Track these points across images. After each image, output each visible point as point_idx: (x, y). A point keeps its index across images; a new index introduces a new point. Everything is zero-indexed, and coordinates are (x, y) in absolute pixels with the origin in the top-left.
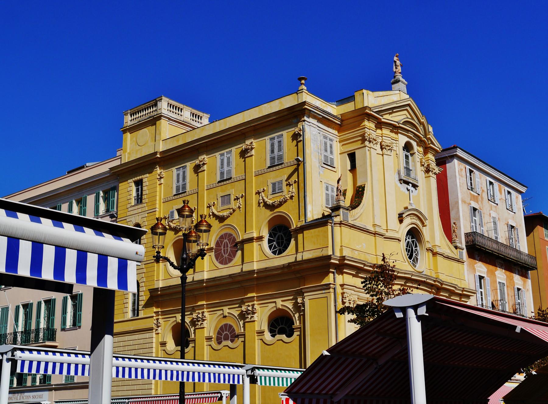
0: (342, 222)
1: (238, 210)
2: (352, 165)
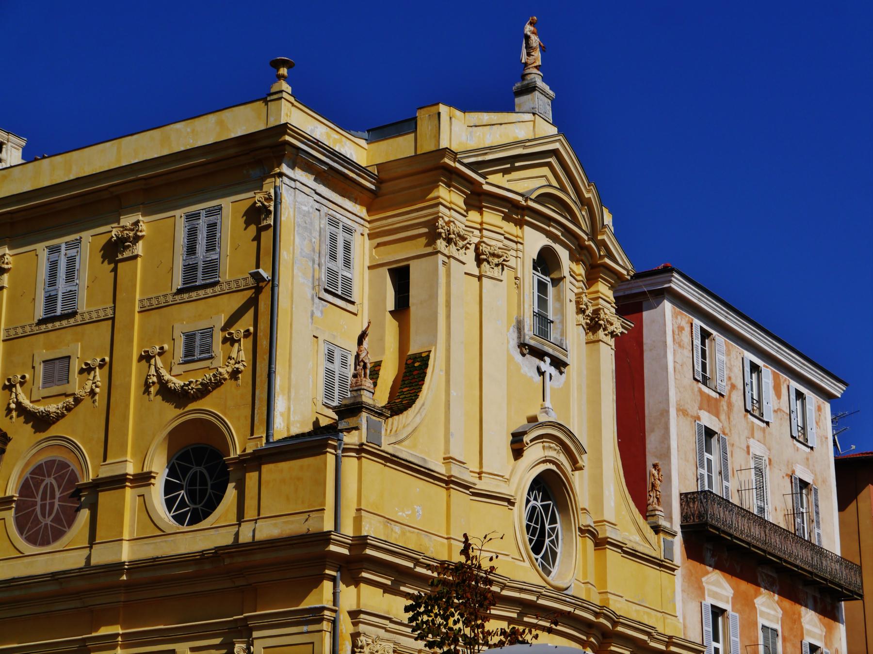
1: (88, 400)
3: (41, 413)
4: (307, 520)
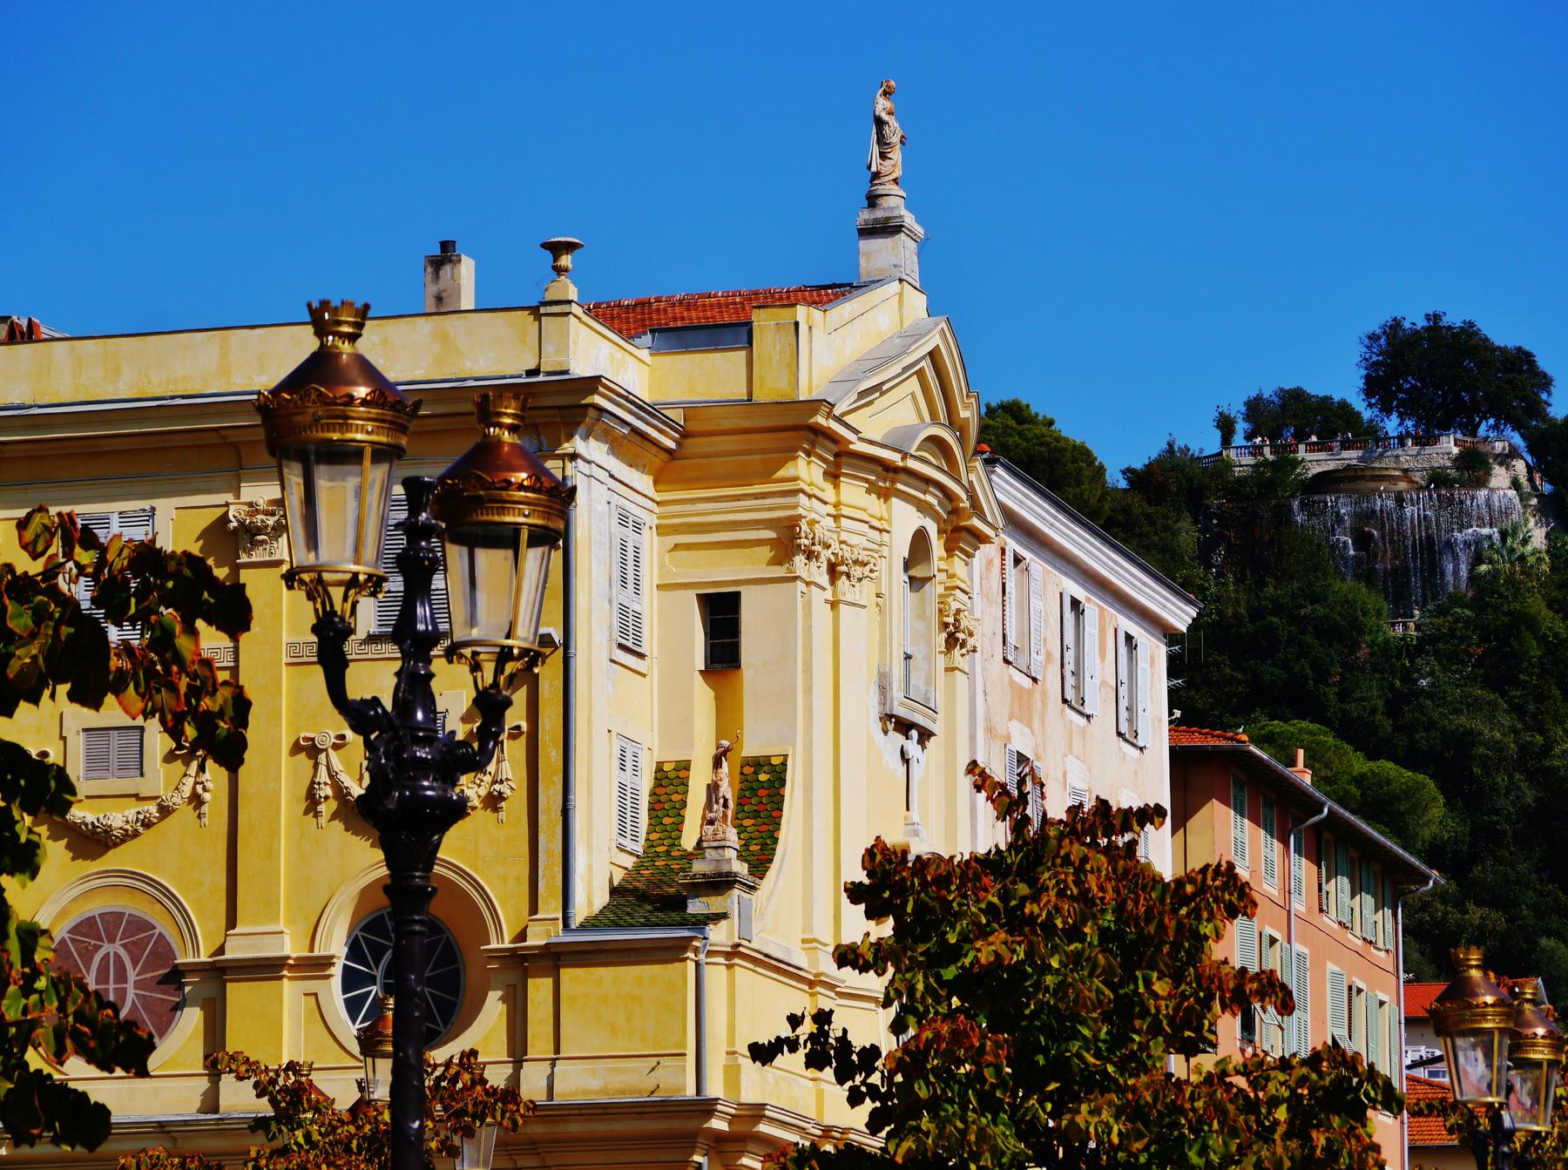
0: (741, 949)
2: (712, 645)
3: (90, 827)
4: (653, 1069)
